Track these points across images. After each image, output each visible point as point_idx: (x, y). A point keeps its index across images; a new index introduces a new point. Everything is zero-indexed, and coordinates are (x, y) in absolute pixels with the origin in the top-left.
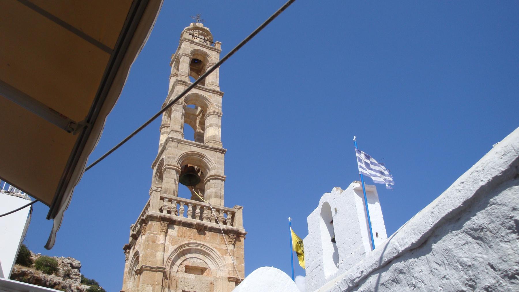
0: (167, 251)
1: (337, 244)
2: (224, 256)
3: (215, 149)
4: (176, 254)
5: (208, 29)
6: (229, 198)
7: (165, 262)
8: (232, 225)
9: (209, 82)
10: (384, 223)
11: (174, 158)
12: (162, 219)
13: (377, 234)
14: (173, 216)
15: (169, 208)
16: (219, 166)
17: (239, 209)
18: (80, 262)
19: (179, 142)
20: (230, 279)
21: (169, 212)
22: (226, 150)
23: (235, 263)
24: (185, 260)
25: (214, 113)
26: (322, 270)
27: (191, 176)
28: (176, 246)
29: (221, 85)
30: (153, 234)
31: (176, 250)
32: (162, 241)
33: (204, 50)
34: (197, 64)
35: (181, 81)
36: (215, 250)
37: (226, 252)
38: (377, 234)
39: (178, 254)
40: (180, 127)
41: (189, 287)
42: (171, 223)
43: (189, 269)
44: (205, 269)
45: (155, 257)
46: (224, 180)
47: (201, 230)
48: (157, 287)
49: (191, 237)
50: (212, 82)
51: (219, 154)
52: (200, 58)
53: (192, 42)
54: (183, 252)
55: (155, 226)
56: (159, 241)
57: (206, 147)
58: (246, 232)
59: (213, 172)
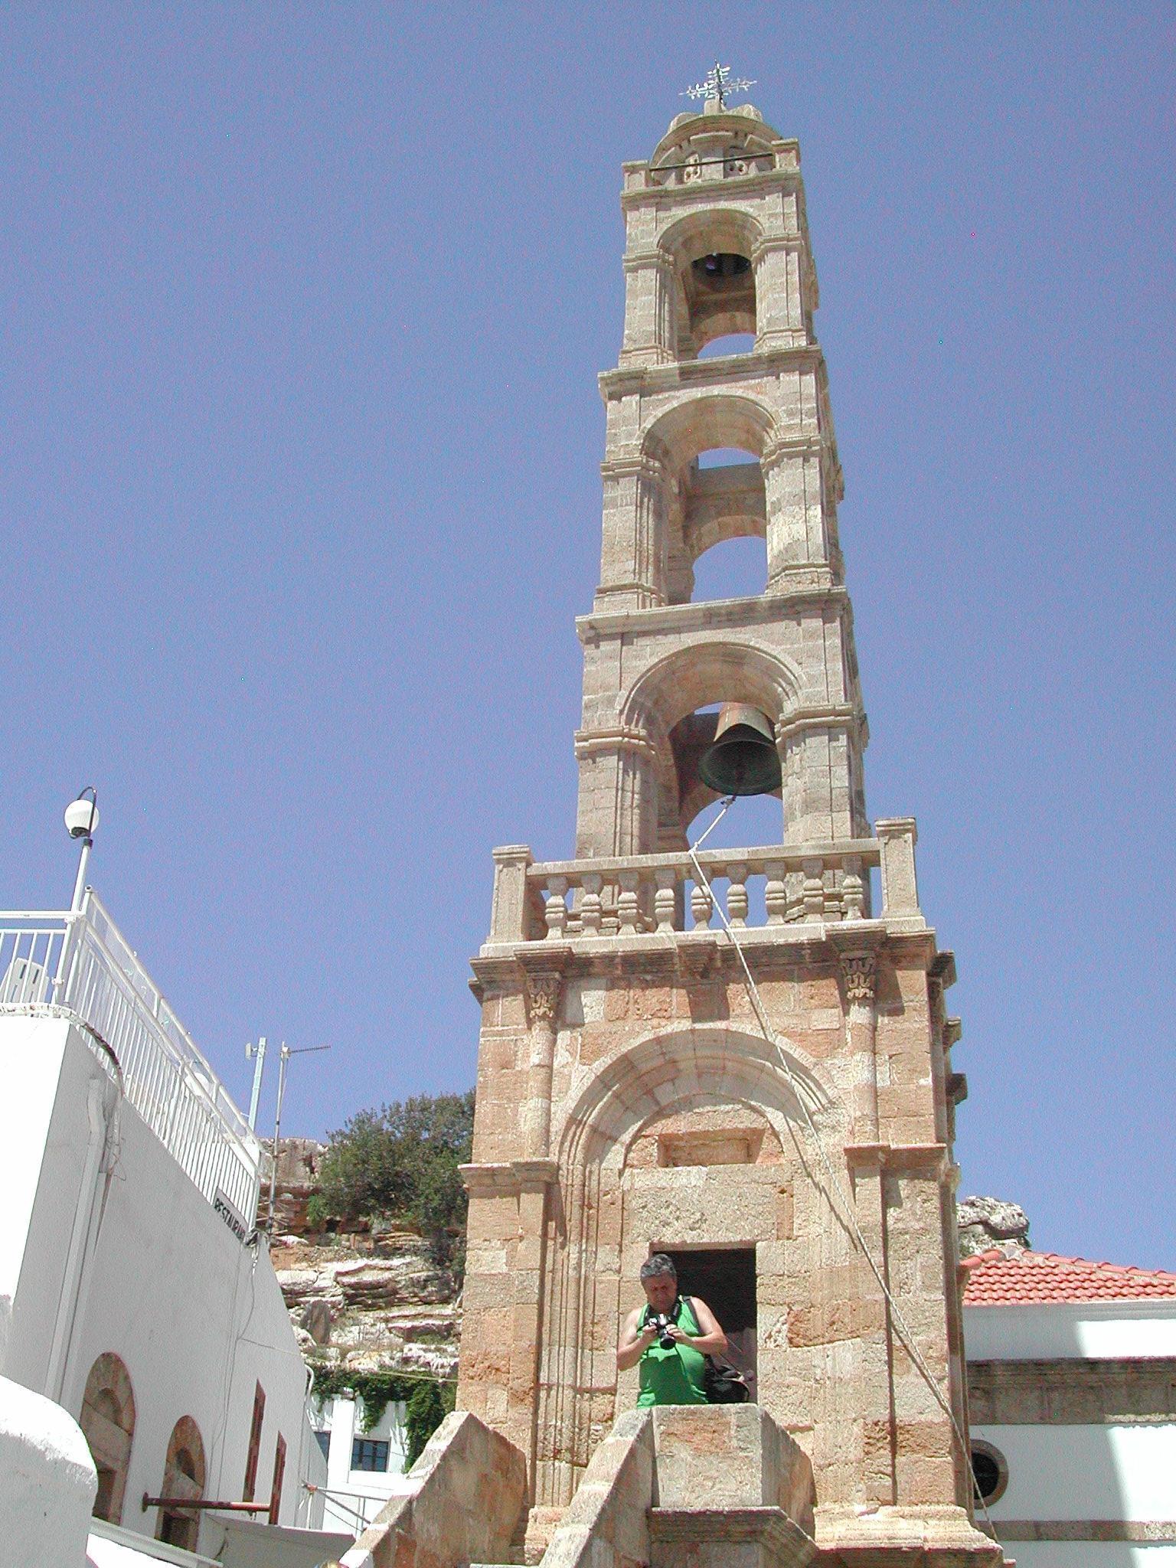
3: (792, 608)
8: (866, 913)
11: (610, 702)
17: (892, 833)
18: (1018, 1208)
19: (626, 634)
20: (859, 1160)
23: (883, 1082)
28: (601, 1064)
30: (500, 1034)
31: (603, 1082)
35: (621, 378)
37: (832, 1041)
39: (616, 1096)
40: (630, 565)
42: (573, 969)
43: (672, 1153)
44: (758, 1134)
45: (516, 1124)
47: (706, 974)
49: (663, 1017)
52: (723, 246)
53: (660, 200)
57: (745, 615)
58: (931, 930)
59: (790, 707)
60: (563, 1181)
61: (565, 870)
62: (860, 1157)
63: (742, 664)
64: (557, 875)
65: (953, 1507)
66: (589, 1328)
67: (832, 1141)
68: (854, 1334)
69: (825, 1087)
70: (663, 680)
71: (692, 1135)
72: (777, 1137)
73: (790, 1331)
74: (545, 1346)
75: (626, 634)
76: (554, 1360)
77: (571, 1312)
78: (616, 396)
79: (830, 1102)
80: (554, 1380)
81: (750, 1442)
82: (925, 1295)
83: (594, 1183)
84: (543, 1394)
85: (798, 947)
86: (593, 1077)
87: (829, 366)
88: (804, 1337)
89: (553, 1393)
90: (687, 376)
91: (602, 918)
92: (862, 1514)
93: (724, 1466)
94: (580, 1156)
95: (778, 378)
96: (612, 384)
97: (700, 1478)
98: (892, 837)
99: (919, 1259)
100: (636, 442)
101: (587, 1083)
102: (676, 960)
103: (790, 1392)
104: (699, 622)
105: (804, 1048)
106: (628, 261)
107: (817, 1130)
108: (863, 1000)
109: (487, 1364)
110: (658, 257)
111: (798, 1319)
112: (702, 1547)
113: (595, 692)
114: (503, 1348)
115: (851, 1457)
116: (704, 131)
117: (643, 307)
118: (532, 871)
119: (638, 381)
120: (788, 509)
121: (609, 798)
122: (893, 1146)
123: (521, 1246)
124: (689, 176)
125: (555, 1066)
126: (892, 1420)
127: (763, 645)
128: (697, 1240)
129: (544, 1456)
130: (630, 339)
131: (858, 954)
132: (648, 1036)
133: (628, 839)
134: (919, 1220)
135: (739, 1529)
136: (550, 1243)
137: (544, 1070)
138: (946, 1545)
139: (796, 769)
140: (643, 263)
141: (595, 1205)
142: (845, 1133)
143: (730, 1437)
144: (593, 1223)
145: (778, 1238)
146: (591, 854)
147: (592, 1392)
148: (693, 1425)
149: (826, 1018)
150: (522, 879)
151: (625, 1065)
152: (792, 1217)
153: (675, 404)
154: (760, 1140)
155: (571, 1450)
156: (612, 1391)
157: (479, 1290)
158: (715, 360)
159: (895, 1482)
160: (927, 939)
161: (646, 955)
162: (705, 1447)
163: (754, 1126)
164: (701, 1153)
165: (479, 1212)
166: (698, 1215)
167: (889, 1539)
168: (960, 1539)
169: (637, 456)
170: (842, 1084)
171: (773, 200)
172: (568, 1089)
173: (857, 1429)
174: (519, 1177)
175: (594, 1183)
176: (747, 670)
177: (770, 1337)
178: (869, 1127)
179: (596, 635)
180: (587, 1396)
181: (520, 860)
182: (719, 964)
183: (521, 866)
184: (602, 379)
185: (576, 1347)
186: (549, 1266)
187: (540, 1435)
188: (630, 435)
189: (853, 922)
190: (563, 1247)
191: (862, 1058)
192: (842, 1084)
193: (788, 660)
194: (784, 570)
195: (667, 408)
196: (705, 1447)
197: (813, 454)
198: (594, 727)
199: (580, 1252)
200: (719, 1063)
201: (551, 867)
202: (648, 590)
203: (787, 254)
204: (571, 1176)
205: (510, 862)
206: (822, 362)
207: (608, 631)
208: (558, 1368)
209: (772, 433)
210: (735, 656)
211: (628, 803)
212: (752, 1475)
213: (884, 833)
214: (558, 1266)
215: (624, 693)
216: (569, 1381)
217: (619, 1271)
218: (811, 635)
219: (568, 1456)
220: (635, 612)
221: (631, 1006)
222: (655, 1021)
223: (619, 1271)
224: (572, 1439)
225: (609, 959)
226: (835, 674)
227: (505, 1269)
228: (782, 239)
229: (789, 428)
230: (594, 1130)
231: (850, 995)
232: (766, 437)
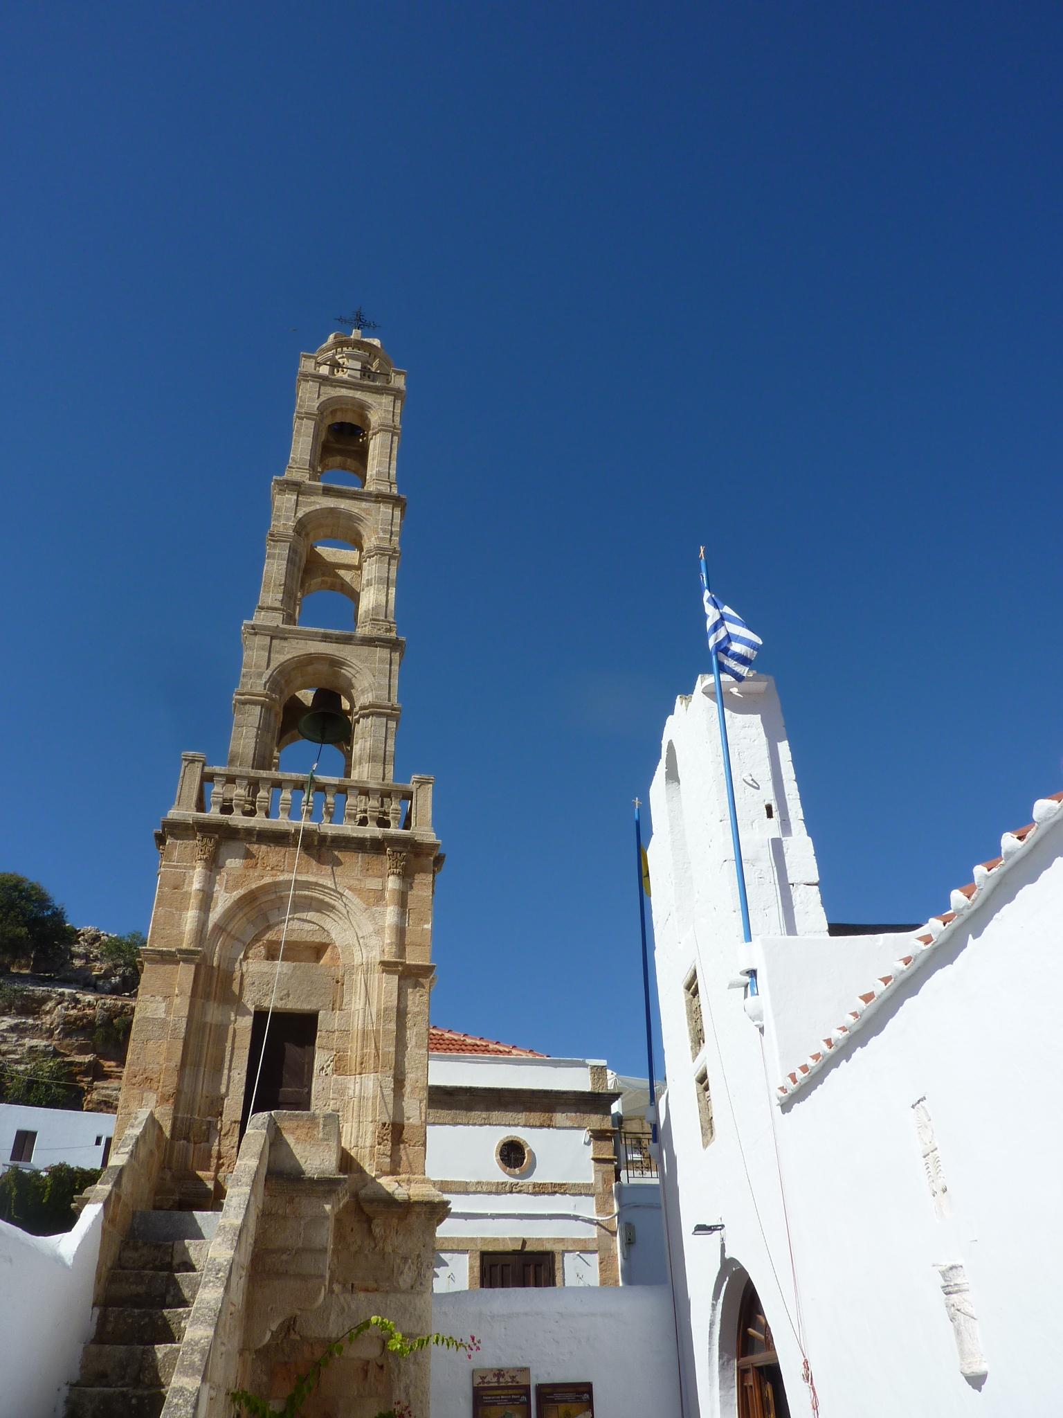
5: (376, 342)
11: (260, 675)
12: (205, 829)
13: (770, 815)
14: (237, 819)
15: (225, 800)
21: (226, 809)
22: (403, 638)
29: (401, 478)
30: (176, 867)
33: (358, 395)
38: (770, 815)
48: (177, 1001)
51: (382, 653)
52: (349, 418)
56: (191, 883)
58: (439, 841)
78: (282, 491)
90: (327, 492)
93: (314, 1150)
101: (228, 904)
117: (302, 445)
118: (207, 769)
138: (421, 1199)
165: (150, 976)
169: (291, 532)
171: (386, 400)
179: (255, 630)
188: (288, 519)
189: (394, 830)
195: (312, 508)
198: (247, 689)
201: (218, 769)
215: (269, 672)
227: (163, 1016)
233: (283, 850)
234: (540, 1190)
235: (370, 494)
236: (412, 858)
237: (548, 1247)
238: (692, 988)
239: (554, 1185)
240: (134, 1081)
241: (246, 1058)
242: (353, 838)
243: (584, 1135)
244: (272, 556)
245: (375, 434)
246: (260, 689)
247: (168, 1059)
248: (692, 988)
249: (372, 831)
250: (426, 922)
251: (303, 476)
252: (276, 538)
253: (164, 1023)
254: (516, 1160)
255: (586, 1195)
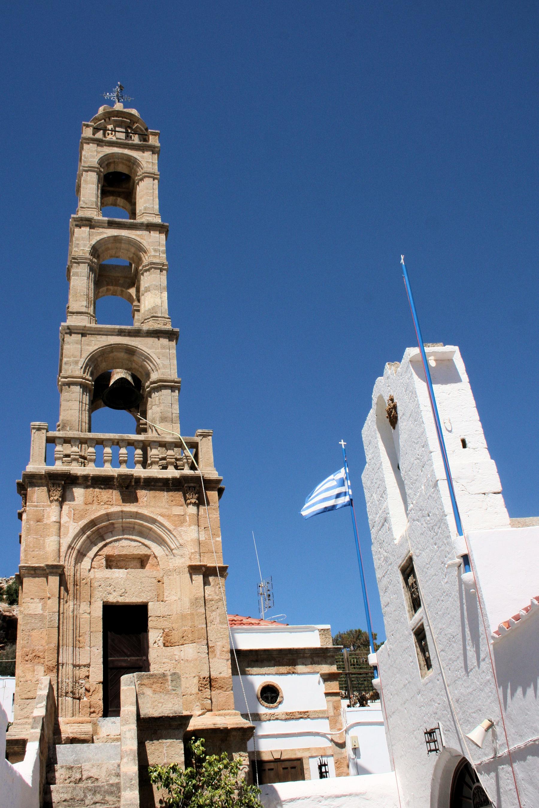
0: (66, 534)
1: (403, 473)
2: (179, 529)
3: (156, 334)
4: (85, 537)
6: (187, 422)
7: (63, 554)
9: (140, 211)
10: (477, 417)
11: (76, 363)
16: (167, 362)
17: (204, 436)
19: (84, 333)
20: (194, 570)
22: (177, 330)
23: (202, 538)
24: (105, 546)
25: (153, 266)
26: (390, 529)
27: (118, 393)
29: (163, 211)
30: (36, 506)
31: (83, 531)
32: (54, 518)
33: (126, 151)
34: (117, 184)
35: (82, 219)
36: (160, 519)
37: (181, 520)
39: (88, 537)
40: (85, 303)
41: (115, 594)
43: (111, 563)
44: (147, 557)
45: (44, 547)
46: (179, 389)
47: (129, 488)
49: (109, 503)
50: (145, 208)
51: (164, 341)
52: (122, 169)
53: (100, 143)
54: (98, 531)
55: (38, 494)
56: (49, 517)
57: (137, 333)
58: (221, 478)
59: (154, 376)
60: (66, 573)
61: (64, 436)
62: (195, 569)
63: (134, 355)
64: (60, 438)
65: (234, 711)
66: (78, 638)
67: (181, 561)
68: (193, 642)
69: (179, 539)
70: (99, 356)
71: (120, 556)
72: (156, 558)
73: (164, 640)
74: (61, 646)
75: (84, 333)
76: (65, 652)
77: (71, 632)
78: (80, 226)
79: (181, 545)
80: (65, 661)
81: (177, 687)
82: (221, 626)
83: (78, 575)
84: (60, 667)
85: (167, 480)
86: (79, 528)
87: (169, 232)
88: (170, 643)
89: (64, 667)
90: (111, 225)
91: (83, 460)
92: (199, 716)
93: (166, 697)
94: (73, 563)
95: (150, 232)
96: (77, 221)
97: (156, 703)
98: (204, 437)
99: (218, 611)
100: (88, 249)
102: (115, 480)
103: (165, 665)
104: (115, 334)
105: (170, 522)
106: (84, 167)
107: (174, 556)
108: (194, 504)
109: (34, 654)
110: (98, 168)
111: (167, 635)
112: (159, 731)
113: (69, 357)
114: (41, 647)
115: (193, 692)
116: (117, 117)
117: (89, 189)
119: (89, 222)
120: (154, 292)
121: (76, 405)
122: (208, 565)
123: (49, 602)
124: (108, 134)
125: (62, 522)
126: (210, 677)
127: (144, 348)
128: (123, 601)
129: (61, 695)
130: (84, 202)
131: (192, 485)
132: (103, 512)
133: (84, 424)
134: (218, 595)
135: (176, 723)
136: (62, 601)
137: (58, 524)
139: (157, 403)
140: (90, 169)
141: (79, 584)
142: (187, 558)
143: (168, 685)
144: (78, 592)
145: (158, 601)
146: (68, 429)
147: (79, 666)
148: (152, 681)
149: (178, 510)
150: (44, 438)
151: (92, 523)
152: (163, 592)
153: (105, 236)
154: (148, 559)
155: (73, 692)
156: (88, 666)
157: (29, 621)
158: (124, 220)
159: (212, 702)
160: (218, 481)
161: (103, 477)
162: (158, 689)
163: (146, 553)
164: (122, 563)
166: (123, 590)
167: (214, 724)
168: (240, 723)
169: (88, 255)
170: (185, 538)
171: (147, 155)
172: (68, 533)
173: (196, 680)
174: (48, 571)
175: (78, 575)
176: (135, 358)
177: (155, 643)
178: (198, 557)
179: (70, 331)
180: (78, 668)
181: (44, 429)
182: (133, 484)
183: (44, 431)
184: (73, 218)
185: (73, 647)
186: (61, 611)
187: (60, 685)
188: (85, 246)
189: (187, 471)
190: (67, 602)
191: (194, 528)
192: (185, 538)
193: (154, 356)
194: (152, 317)
196: (158, 689)
197: (164, 269)
199: (74, 605)
200: (132, 526)
201: (57, 434)
202: (91, 316)
203: (154, 180)
204: (69, 572)
205: (39, 429)
206: (168, 231)
207: (75, 331)
208: (66, 656)
209: (147, 257)
210: (131, 351)
211: (84, 409)
212: (179, 701)
213: (200, 435)
214: (65, 611)
215: (83, 360)
216: (71, 662)
217: (90, 613)
218: (163, 347)
219: (71, 695)
220: (88, 325)
221: (95, 498)
222: (106, 506)
223: (90, 613)
224: (73, 688)
225: (86, 478)
226: (174, 365)
227: (41, 612)
228: (152, 174)
229: (155, 256)
230: (79, 551)
231: (188, 501)
232: (143, 258)
233: (111, 491)
234: (290, 717)
235: (142, 224)
236: (192, 488)
237: (299, 755)
238: (408, 570)
239: (300, 713)
240: (27, 658)
241: (101, 638)
242: (160, 479)
243: (317, 677)
244: (76, 274)
245: (142, 180)
246: (78, 372)
247: (49, 643)
248: (408, 570)
249: (171, 473)
250: (219, 537)
251: (95, 215)
252: (77, 261)
253: (42, 617)
254: (272, 698)
255: (322, 718)
